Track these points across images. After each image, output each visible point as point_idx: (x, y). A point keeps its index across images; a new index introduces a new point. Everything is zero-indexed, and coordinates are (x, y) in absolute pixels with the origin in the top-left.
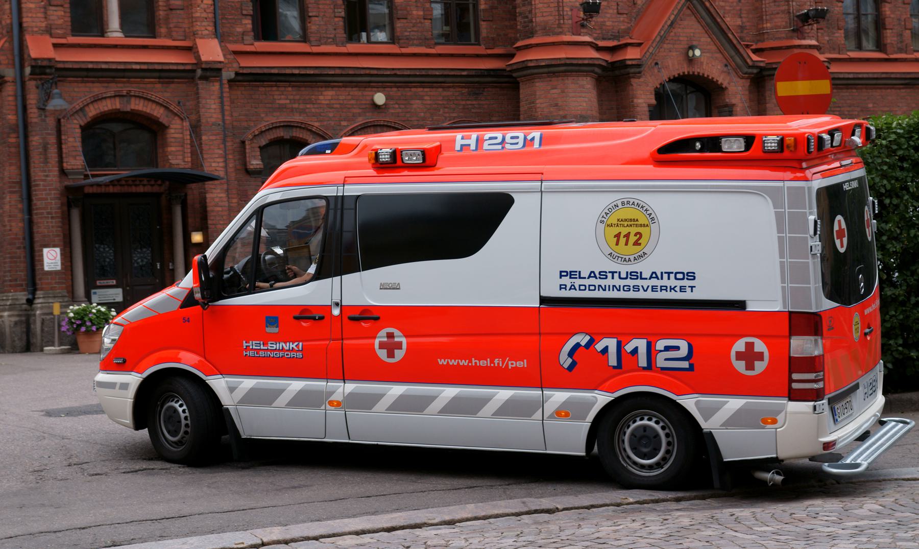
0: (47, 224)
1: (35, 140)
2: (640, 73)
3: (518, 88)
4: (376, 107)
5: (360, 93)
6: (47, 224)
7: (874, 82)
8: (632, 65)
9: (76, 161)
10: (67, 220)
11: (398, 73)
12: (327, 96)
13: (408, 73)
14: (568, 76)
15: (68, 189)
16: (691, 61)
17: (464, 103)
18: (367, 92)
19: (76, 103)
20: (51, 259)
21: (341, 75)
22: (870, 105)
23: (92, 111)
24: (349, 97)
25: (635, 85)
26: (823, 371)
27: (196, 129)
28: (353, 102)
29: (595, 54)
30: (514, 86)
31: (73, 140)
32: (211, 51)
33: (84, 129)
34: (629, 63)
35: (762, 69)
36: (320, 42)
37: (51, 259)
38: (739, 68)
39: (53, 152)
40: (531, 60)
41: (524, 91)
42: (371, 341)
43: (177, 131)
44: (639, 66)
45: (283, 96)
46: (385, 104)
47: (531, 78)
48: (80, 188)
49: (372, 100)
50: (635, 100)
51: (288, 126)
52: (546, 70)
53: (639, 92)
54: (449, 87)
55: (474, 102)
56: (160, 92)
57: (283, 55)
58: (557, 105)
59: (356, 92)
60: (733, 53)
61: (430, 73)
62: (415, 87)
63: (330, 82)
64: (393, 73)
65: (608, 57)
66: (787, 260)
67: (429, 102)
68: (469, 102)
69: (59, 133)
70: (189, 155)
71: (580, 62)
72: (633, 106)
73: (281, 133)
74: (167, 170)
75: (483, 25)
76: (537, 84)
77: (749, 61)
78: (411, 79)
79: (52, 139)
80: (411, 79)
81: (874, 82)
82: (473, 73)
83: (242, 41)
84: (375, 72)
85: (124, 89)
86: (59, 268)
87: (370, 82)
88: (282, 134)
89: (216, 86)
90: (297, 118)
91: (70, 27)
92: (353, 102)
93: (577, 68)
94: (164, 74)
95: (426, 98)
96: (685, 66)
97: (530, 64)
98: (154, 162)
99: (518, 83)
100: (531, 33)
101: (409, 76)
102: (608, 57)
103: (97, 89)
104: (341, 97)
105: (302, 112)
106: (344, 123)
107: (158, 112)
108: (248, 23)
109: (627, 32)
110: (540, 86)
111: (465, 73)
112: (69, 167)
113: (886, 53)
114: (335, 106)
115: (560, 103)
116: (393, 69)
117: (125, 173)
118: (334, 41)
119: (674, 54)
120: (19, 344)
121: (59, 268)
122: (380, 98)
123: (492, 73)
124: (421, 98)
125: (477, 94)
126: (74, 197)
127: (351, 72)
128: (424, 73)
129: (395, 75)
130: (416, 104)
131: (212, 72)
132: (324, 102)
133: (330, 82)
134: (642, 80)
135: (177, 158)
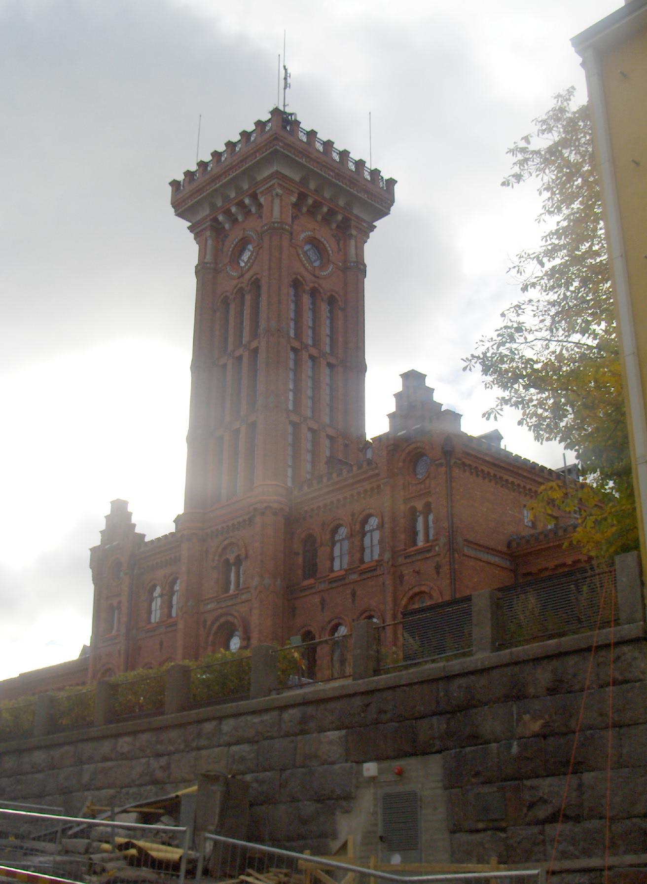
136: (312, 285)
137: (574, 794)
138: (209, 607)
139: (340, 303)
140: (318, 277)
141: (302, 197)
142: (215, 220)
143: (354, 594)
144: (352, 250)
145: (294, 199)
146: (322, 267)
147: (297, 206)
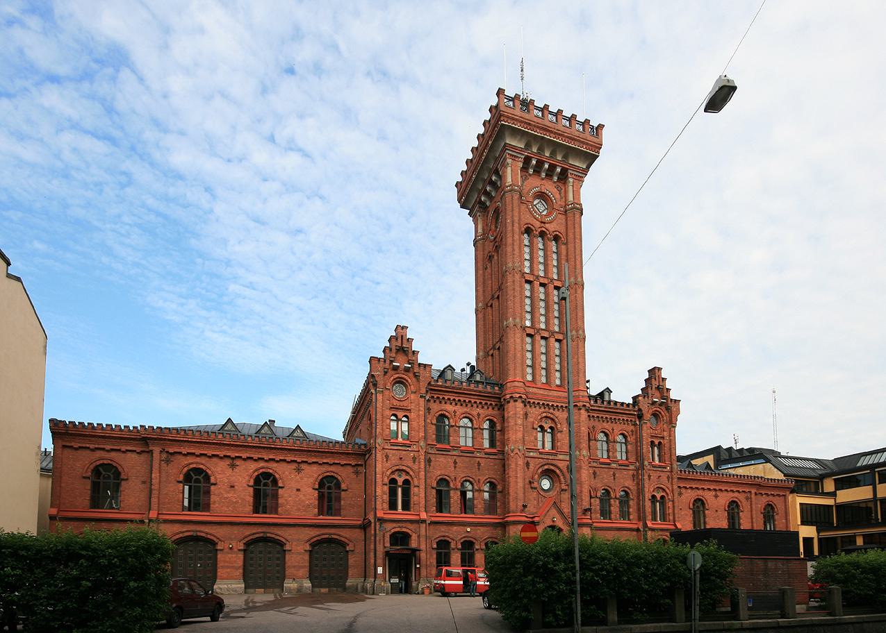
0: (379, 561)
1: (378, 538)
3: (505, 528)
6: (379, 561)
9: (388, 544)
10: (384, 559)
15: (386, 552)
16: (554, 521)
19: (391, 528)
20: (380, 570)
23: (393, 531)
26: (619, 622)
27: (419, 537)
29: (526, 519)
30: (505, 527)
31: (387, 539)
32: (424, 516)
33: (390, 536)
36: (453, 514)
37: (380, 570)
39: (382, 541)
41: (507, 528)
43: (414, 537)
45: (443, 528)
47: (509, 525)
48: (388, 551)
51: (444, 536)
56: (410, 526)
57: (444, 517)
59: (462, 527)
65: (531, 520)
69: (384, 537)
74: (410, 547)
75: (498, 510)
79: (382, 538)
83: (432, 513)
85: (401, 525)
86: (815, 527)
89: (424, 525)
90: (447, 534)
94: (411, 522)
98: (408, 545)
100: (509, 513)
102: (531, 520)
103: (395, 525)
105: (448, 532)
107: (409, 532)
108: (435, 508)
109: (536, 513)
110: (511, 527)
112: (218, 591)
117: (399, 548)
118: (457, 514)
120: (371, 593)
121: (815, 527)
122: (469, 530)
126: (387, 553)
131: (424, 521)
135: (414, 545)
136: (539, 230)
137: (508, 396)
138: (532, 454)
139: (563, 239)
140: (544, 223)
141: (527, 160)
142: (480, 202)
143: (614, 475)
144: (571, 198)
145: (521, 165)
146: (548, 215)
147: (525, 168)
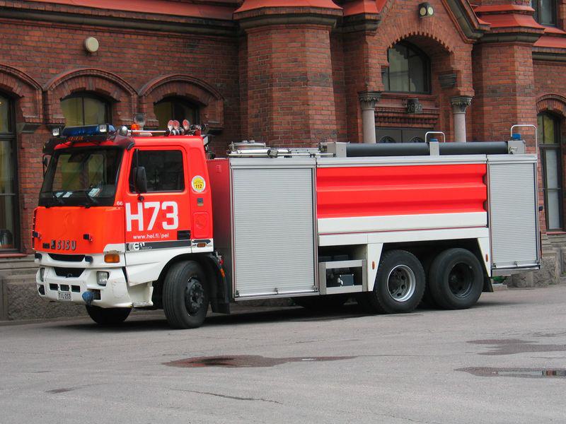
2: (375, 29)
4: (87, 52)
5: (70, 36)
7: (554, 57)
8: (371, 20)
11: (114, 15)
12: (35, 36)
13: (124, 15)
14: (308, 28)
17: (178, 55)
18: (78, 36)
21: (52, 13)
22: (549, 82)
24: (59, 40)
25: (369, 43)
28: (63, 46)
34: (367, 17)
35: (486, 34)
38: (464, 29)
40: (269, 8)
42: (32, 275)
44: (375, 21)
46: (97, 52)
47: (269, 28)
49: (84, 46)
50: (370, 60)
52: (285, 20)
53: (374, 51)
54: (164, 36)
55: (189, 56)
58: (296, 60)
59: (64, 34)
60: (460, 14)
61: (147, 17)
62: (129, 33)
63: (38, 20)
64: (108, 14)
66: (316, 189)
67: (142, 52)
68: (183, 55)
70: (5, 84)
71: (324, 12)
72: (367, 66)
73: (80, 84)
76: (273, 36)
77: (476, 24)
78: (126, 24)
80: (126, 24)
81: (554, 57)
82: (191, 21)
84: (89, 12)
87: (82, 24)
88: (175, 90)
91: (421, 297)
92: (63, 46)
93: (319, 19)
95: (140, 46)
96: (416, 25)
97: (268, 12)
99: (245, 35)
101: (124, 19)
104: (49, 40)
106: (52, 71)
111: (183, 21)
113: (562, 29)
114: (43, 49)
115: (300, 58)
116: (109, 10)
119: (406, 11)
122: (93, 44)
123: (210, 23)
124: (135, 47)
125: (192, 46)
127: (63, 10)
128: (140, 17)
129: (111, 17)
130: (130, 53)
132: (30, 44)
133: (38, 20)
134: (376, 37)
